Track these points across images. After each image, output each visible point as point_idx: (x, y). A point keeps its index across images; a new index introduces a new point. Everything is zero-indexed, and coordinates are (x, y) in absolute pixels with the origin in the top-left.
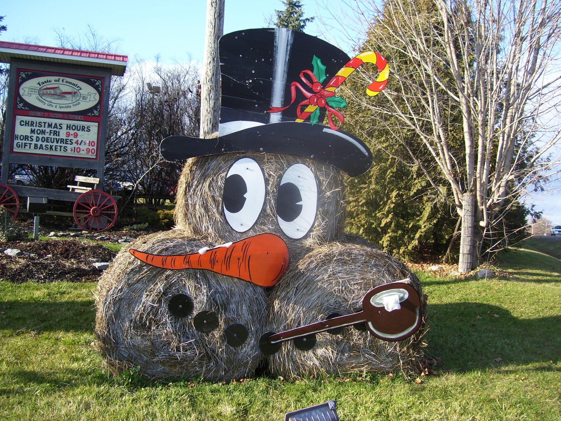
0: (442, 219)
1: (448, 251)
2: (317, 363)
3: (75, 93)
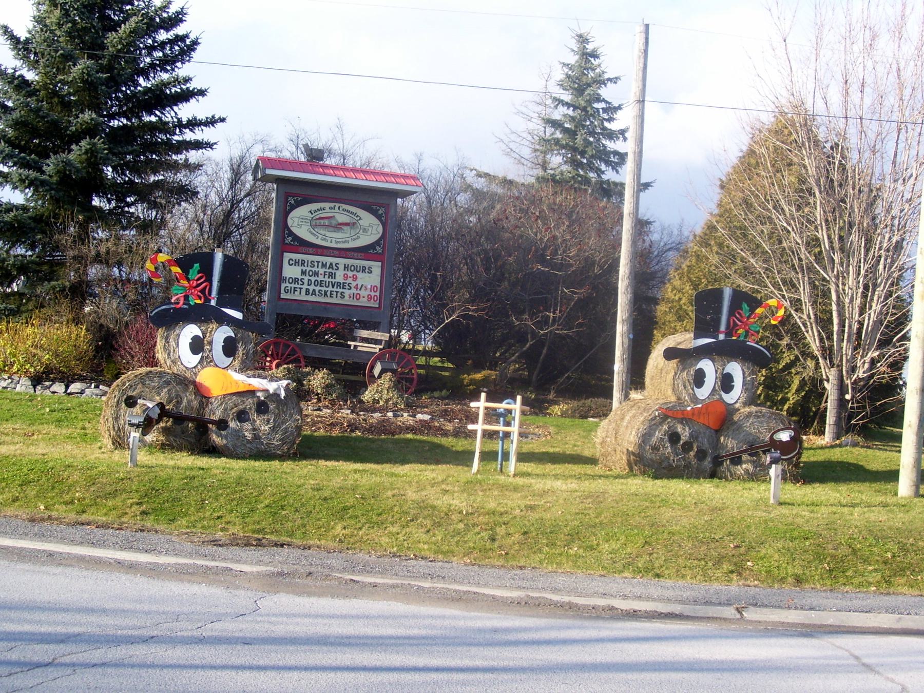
0: (810, 391)
1: (815, 423)
2: (743, 472)
3: (354, 224)
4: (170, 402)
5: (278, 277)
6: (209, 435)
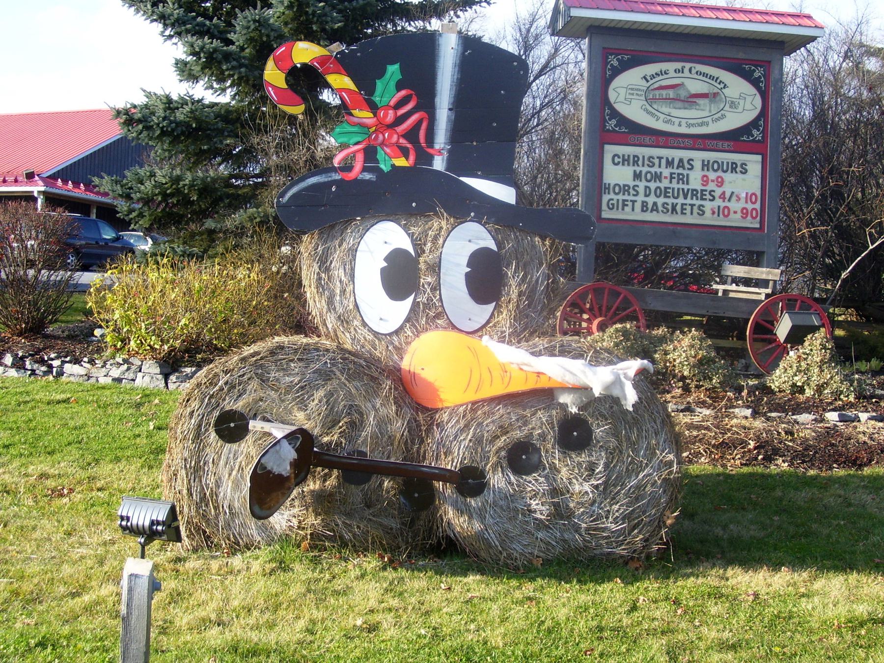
3: (715, 95)
4: (330, 424)
5: (597, 185)
6: (437, 509)
